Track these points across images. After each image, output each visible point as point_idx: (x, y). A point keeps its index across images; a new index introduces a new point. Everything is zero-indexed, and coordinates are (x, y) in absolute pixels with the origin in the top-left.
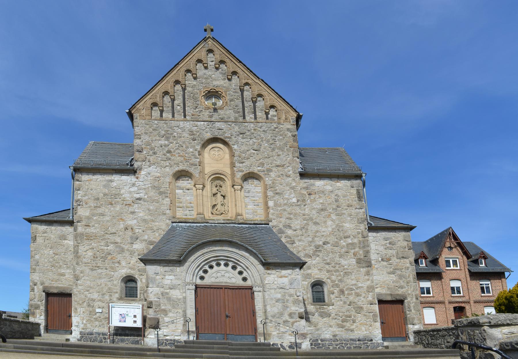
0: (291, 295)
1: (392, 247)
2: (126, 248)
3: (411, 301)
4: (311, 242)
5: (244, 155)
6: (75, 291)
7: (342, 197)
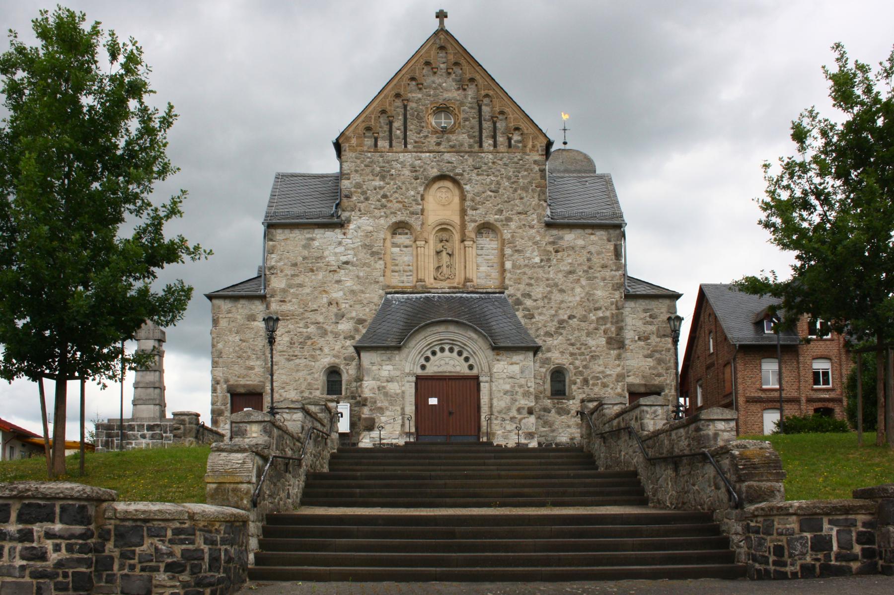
0: (521, 386)
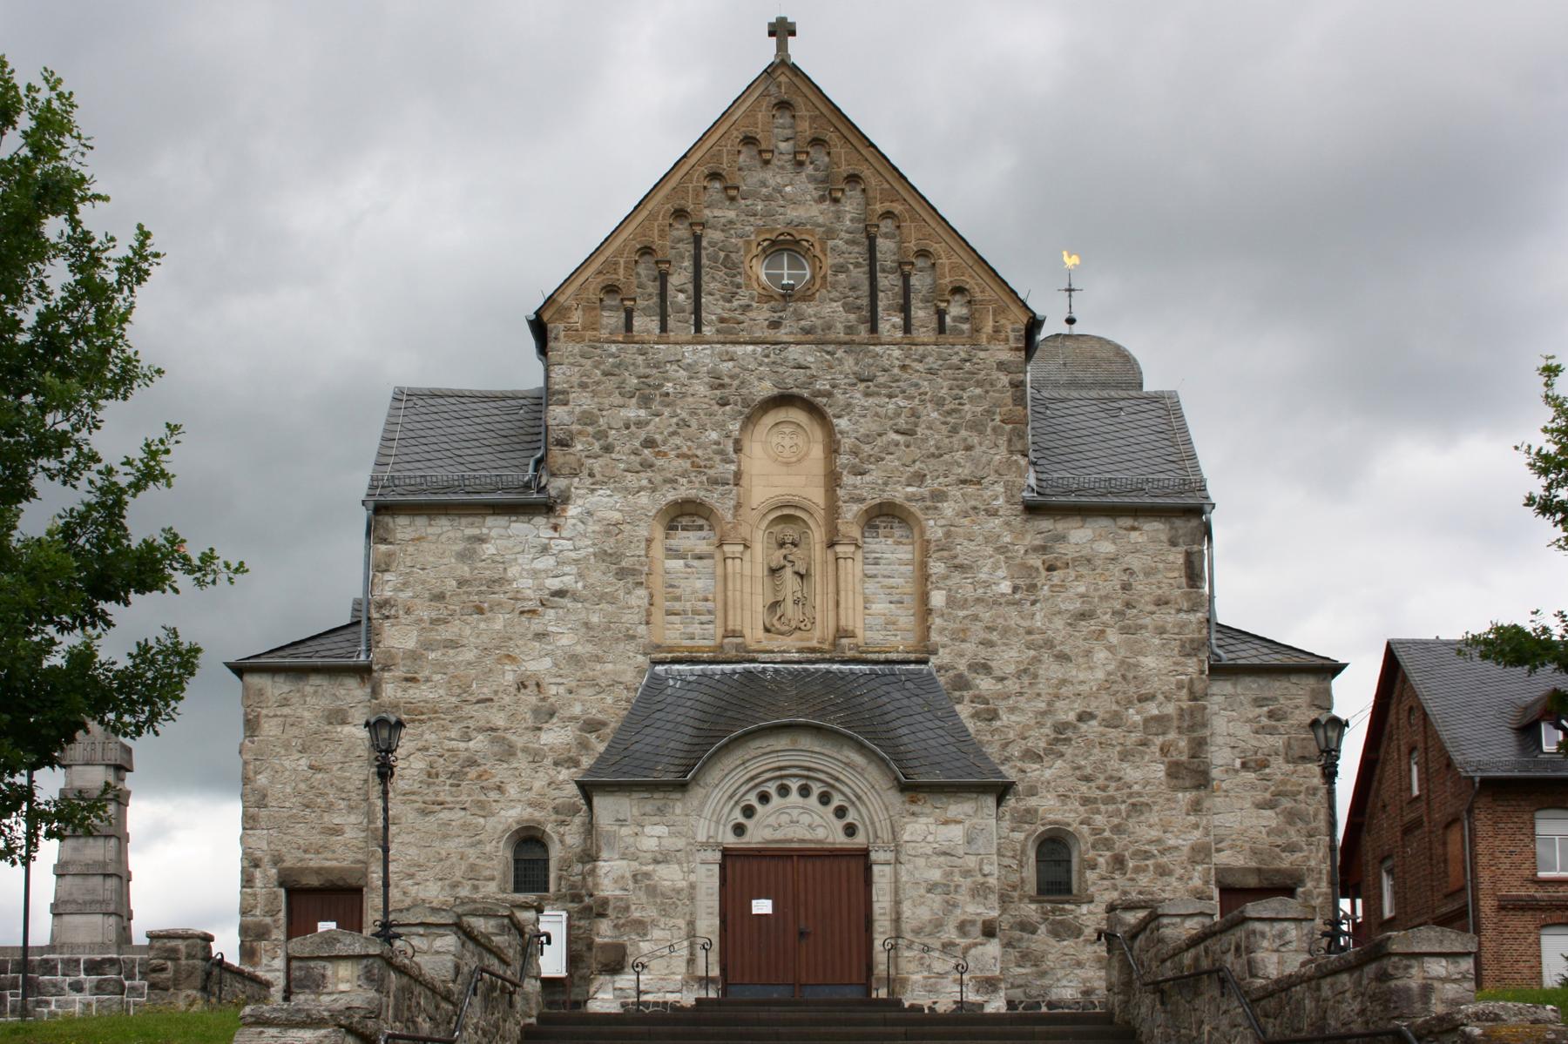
0: (967, 873)
1: (1275, 728)
2: (520, 745)
3: (1316, 892)
4: (1044, 714)
5: (867, 448)
7: (1141, 576)
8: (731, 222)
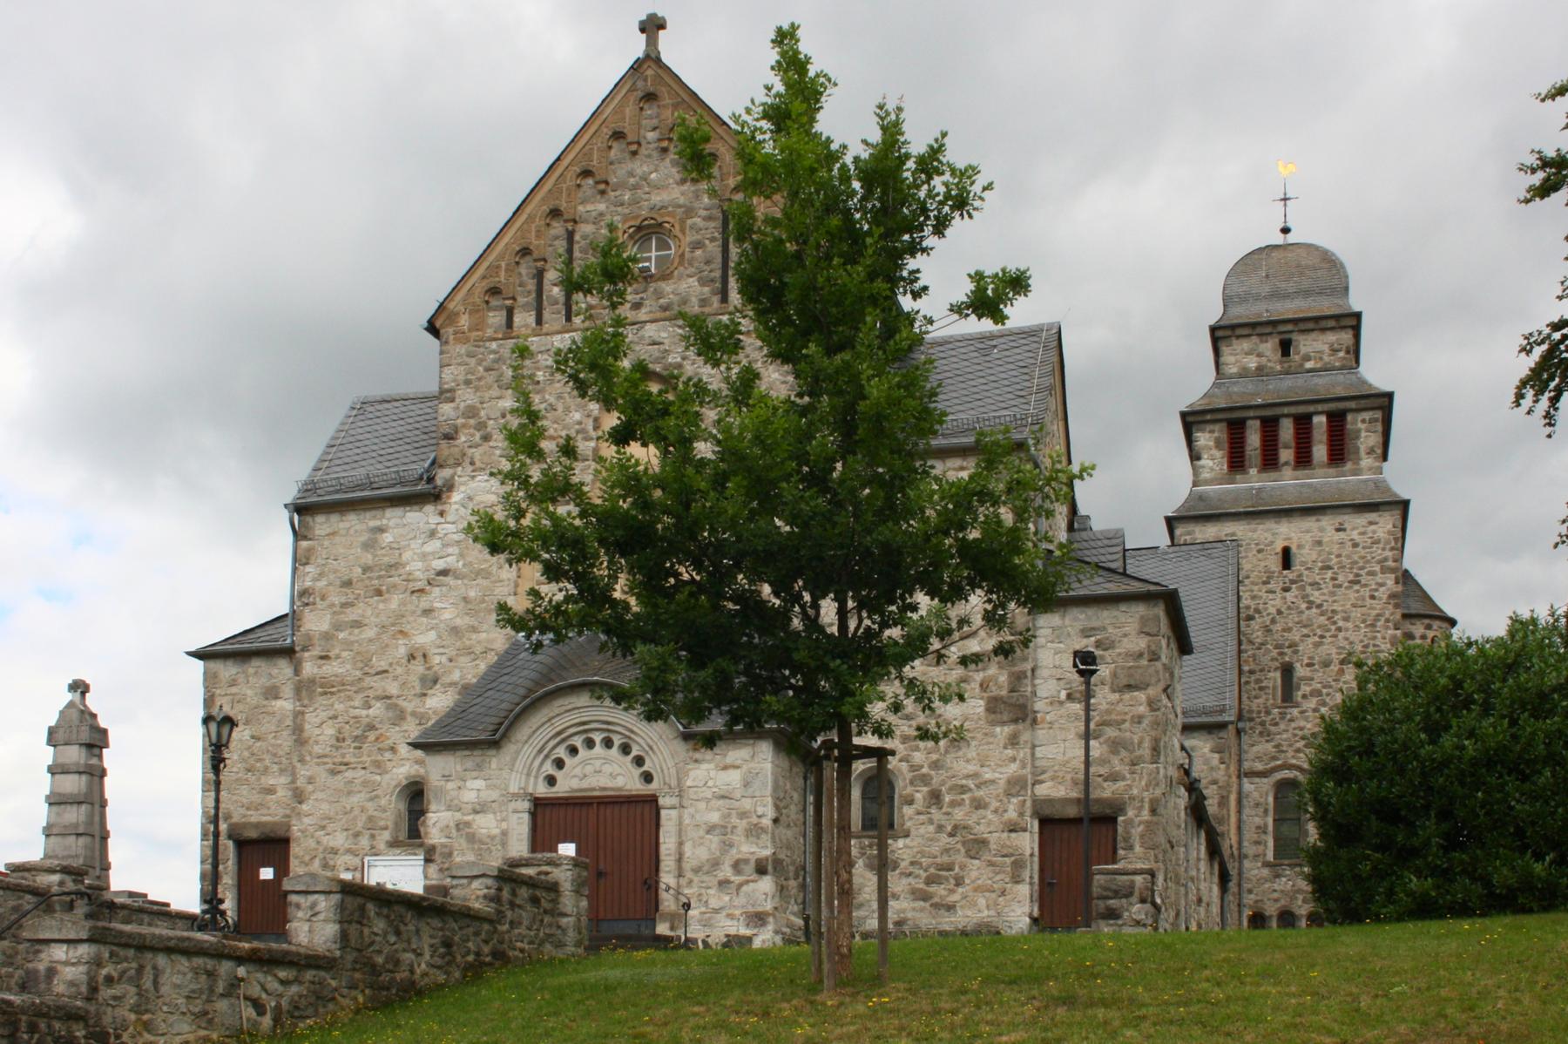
0: (743, 815)
6: (295, 830)
8: (601, 214)
